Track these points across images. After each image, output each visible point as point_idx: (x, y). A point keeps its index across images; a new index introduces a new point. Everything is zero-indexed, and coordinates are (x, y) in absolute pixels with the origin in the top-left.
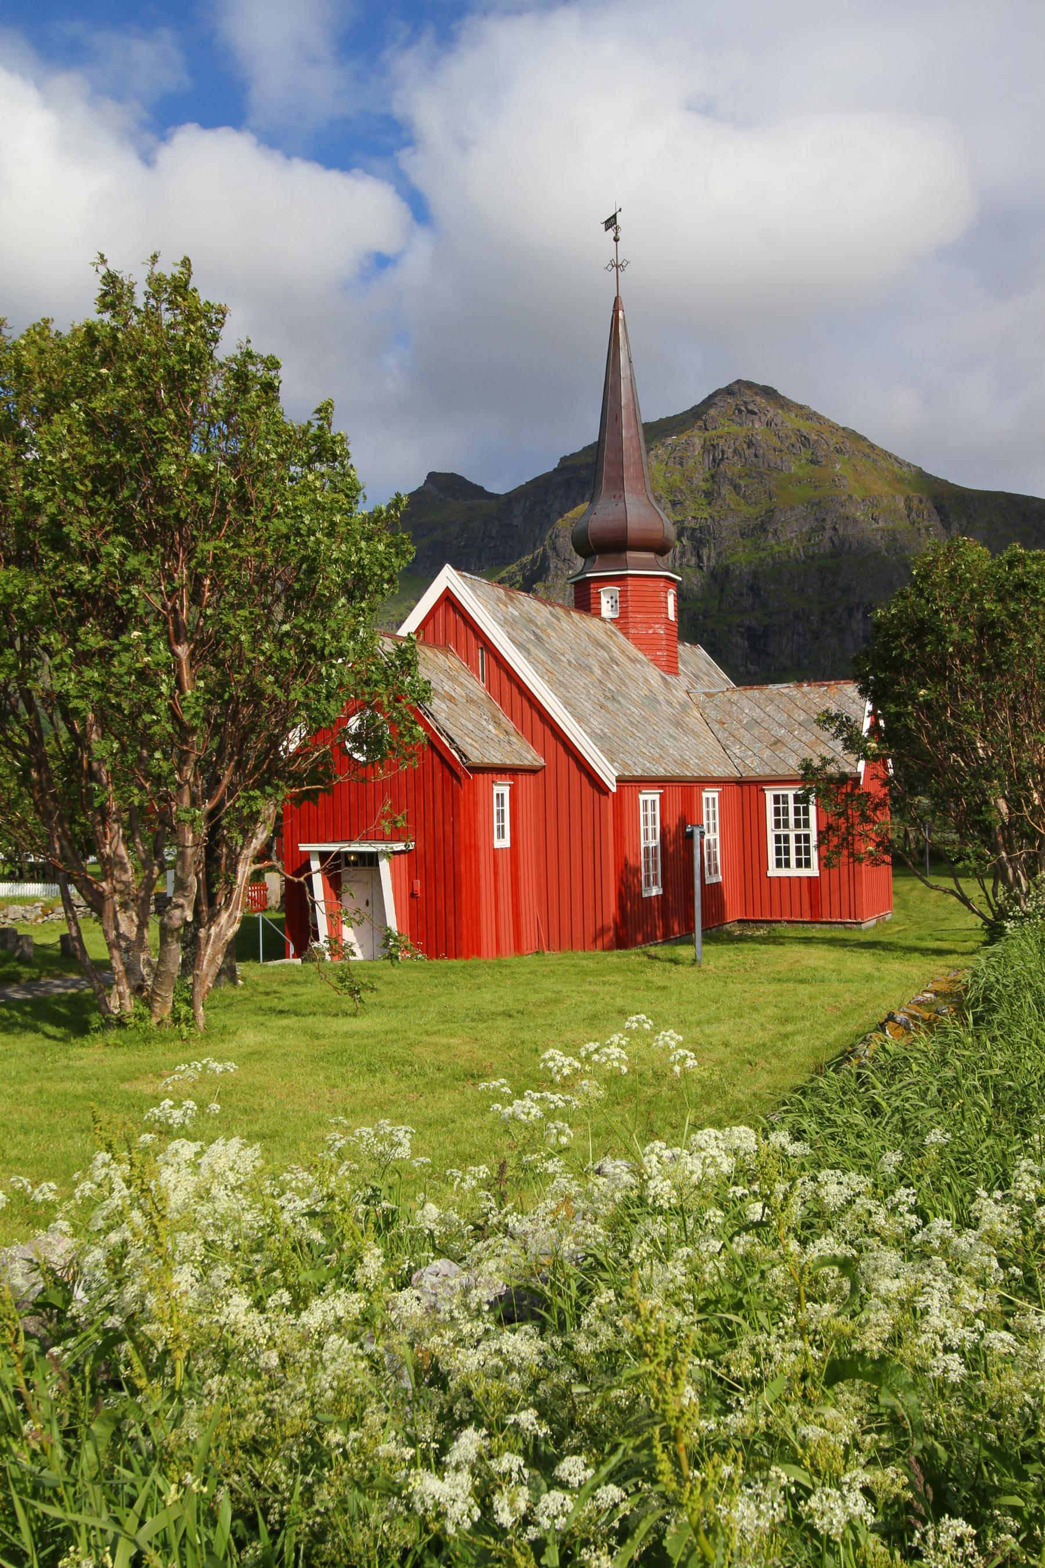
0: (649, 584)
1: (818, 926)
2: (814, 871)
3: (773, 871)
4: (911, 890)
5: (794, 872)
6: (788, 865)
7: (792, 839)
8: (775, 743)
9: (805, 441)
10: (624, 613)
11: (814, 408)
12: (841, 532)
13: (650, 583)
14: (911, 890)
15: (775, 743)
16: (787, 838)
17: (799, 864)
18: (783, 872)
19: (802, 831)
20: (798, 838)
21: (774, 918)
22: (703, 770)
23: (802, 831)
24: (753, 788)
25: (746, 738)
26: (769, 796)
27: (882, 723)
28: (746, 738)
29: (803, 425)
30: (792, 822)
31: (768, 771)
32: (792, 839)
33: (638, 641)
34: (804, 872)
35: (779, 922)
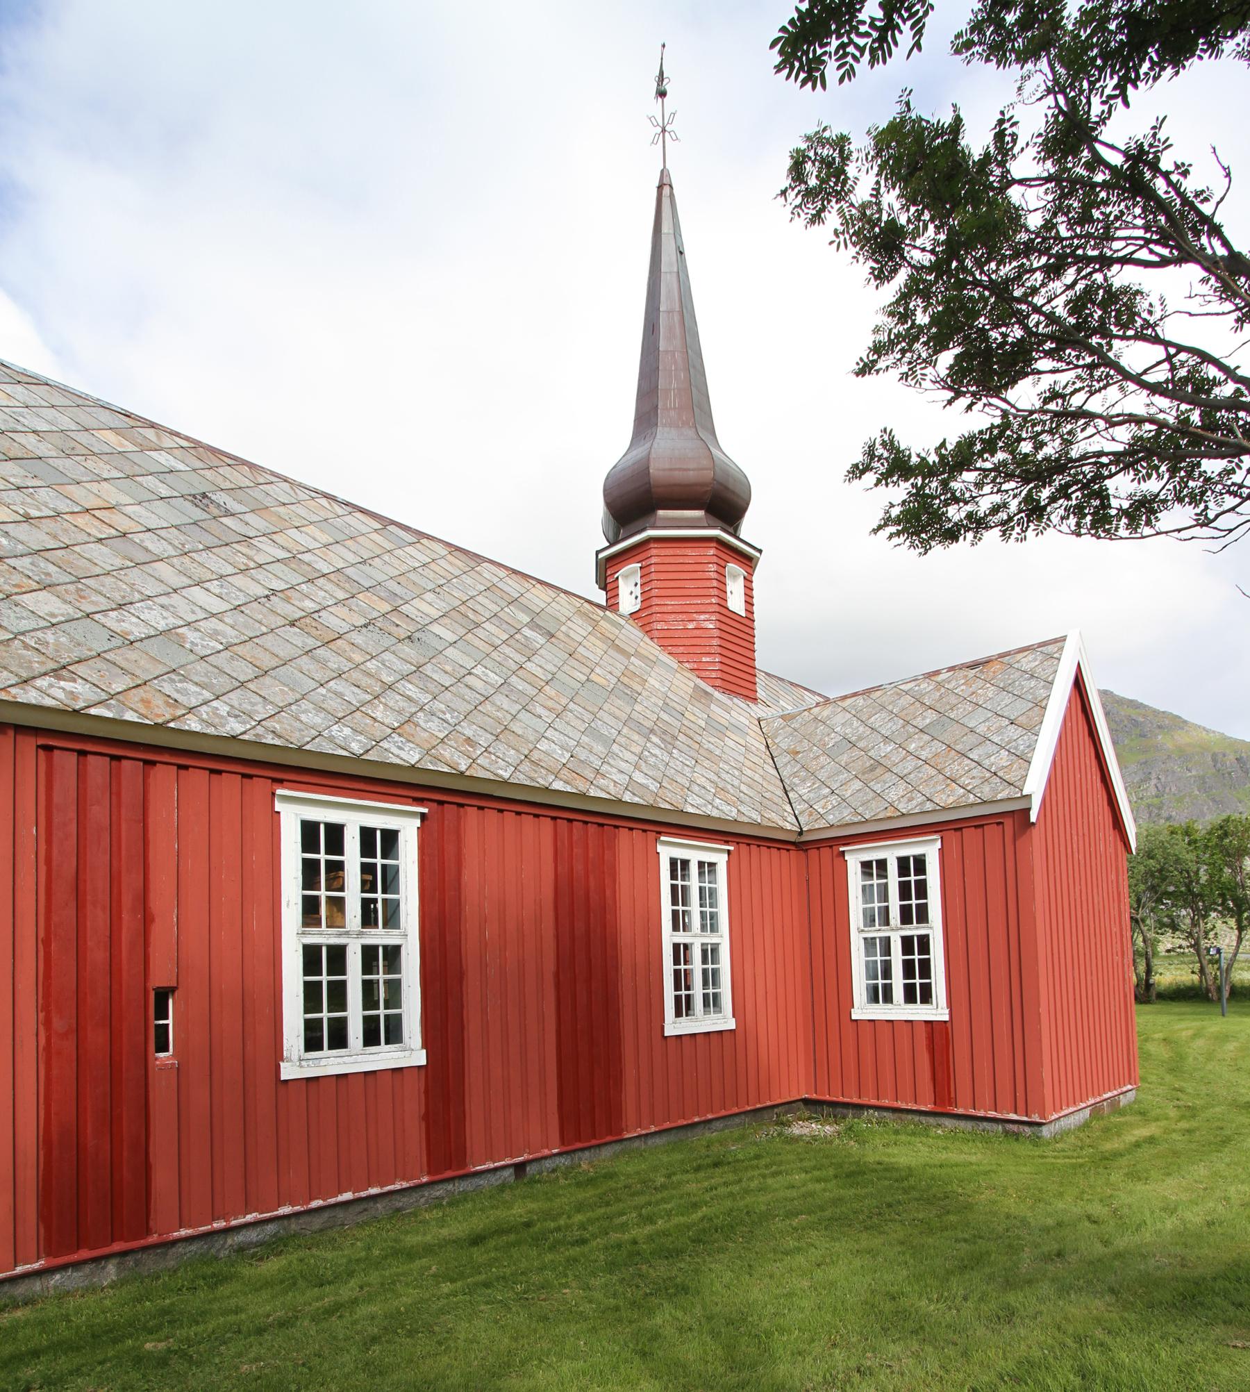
0: (689, 552)
1: (949, 1123)
2: (937, 1010)
3: (863, 1010)
4: (1195, 1036)
5: (899, 1011)
6: (888, 998)
7: (896, 947)
8: (872, 769)
9: (1135, 723)
10: (646, 598)
11: (1140, 701)
12: (1163, 780)
13: (691, 552)
14: (1195, 1036)
15: (872, 769)
16: (338, 956)
17: (910, 997)
18: (880, 1012)
19: (914, 930)
20: (907, 943)
21: (864, 1101)
22: (532, 779)
23: (914, 930)
24: (826, 852)
25: (826, 767)
26: (853, 862)
27: (833, 27)
28: (826, 767)
29: (1133, 713)
30: (895, 914)
31: (847, 815)
32: (354, 961)
33: (667, 642)
34: (919, 1012)
35: (861, 1107)
